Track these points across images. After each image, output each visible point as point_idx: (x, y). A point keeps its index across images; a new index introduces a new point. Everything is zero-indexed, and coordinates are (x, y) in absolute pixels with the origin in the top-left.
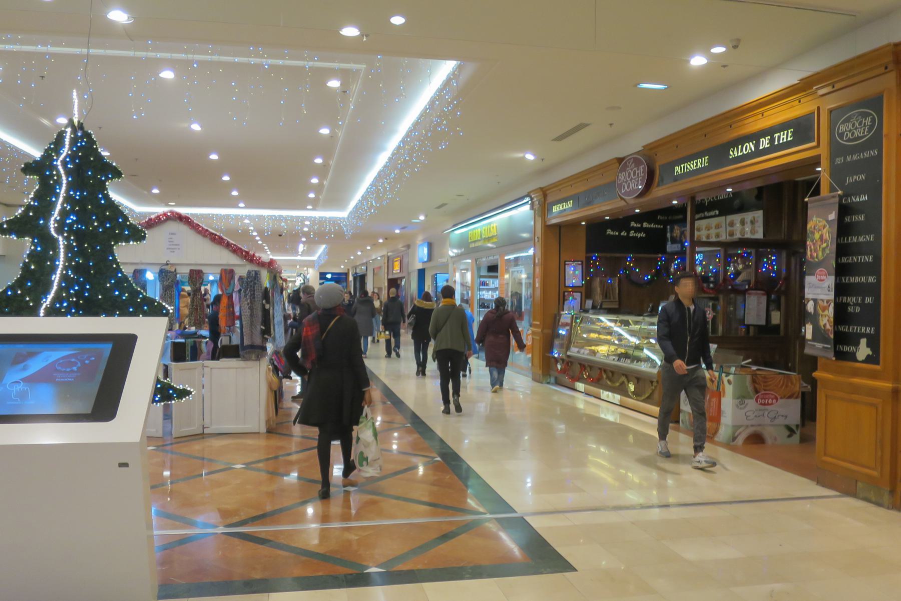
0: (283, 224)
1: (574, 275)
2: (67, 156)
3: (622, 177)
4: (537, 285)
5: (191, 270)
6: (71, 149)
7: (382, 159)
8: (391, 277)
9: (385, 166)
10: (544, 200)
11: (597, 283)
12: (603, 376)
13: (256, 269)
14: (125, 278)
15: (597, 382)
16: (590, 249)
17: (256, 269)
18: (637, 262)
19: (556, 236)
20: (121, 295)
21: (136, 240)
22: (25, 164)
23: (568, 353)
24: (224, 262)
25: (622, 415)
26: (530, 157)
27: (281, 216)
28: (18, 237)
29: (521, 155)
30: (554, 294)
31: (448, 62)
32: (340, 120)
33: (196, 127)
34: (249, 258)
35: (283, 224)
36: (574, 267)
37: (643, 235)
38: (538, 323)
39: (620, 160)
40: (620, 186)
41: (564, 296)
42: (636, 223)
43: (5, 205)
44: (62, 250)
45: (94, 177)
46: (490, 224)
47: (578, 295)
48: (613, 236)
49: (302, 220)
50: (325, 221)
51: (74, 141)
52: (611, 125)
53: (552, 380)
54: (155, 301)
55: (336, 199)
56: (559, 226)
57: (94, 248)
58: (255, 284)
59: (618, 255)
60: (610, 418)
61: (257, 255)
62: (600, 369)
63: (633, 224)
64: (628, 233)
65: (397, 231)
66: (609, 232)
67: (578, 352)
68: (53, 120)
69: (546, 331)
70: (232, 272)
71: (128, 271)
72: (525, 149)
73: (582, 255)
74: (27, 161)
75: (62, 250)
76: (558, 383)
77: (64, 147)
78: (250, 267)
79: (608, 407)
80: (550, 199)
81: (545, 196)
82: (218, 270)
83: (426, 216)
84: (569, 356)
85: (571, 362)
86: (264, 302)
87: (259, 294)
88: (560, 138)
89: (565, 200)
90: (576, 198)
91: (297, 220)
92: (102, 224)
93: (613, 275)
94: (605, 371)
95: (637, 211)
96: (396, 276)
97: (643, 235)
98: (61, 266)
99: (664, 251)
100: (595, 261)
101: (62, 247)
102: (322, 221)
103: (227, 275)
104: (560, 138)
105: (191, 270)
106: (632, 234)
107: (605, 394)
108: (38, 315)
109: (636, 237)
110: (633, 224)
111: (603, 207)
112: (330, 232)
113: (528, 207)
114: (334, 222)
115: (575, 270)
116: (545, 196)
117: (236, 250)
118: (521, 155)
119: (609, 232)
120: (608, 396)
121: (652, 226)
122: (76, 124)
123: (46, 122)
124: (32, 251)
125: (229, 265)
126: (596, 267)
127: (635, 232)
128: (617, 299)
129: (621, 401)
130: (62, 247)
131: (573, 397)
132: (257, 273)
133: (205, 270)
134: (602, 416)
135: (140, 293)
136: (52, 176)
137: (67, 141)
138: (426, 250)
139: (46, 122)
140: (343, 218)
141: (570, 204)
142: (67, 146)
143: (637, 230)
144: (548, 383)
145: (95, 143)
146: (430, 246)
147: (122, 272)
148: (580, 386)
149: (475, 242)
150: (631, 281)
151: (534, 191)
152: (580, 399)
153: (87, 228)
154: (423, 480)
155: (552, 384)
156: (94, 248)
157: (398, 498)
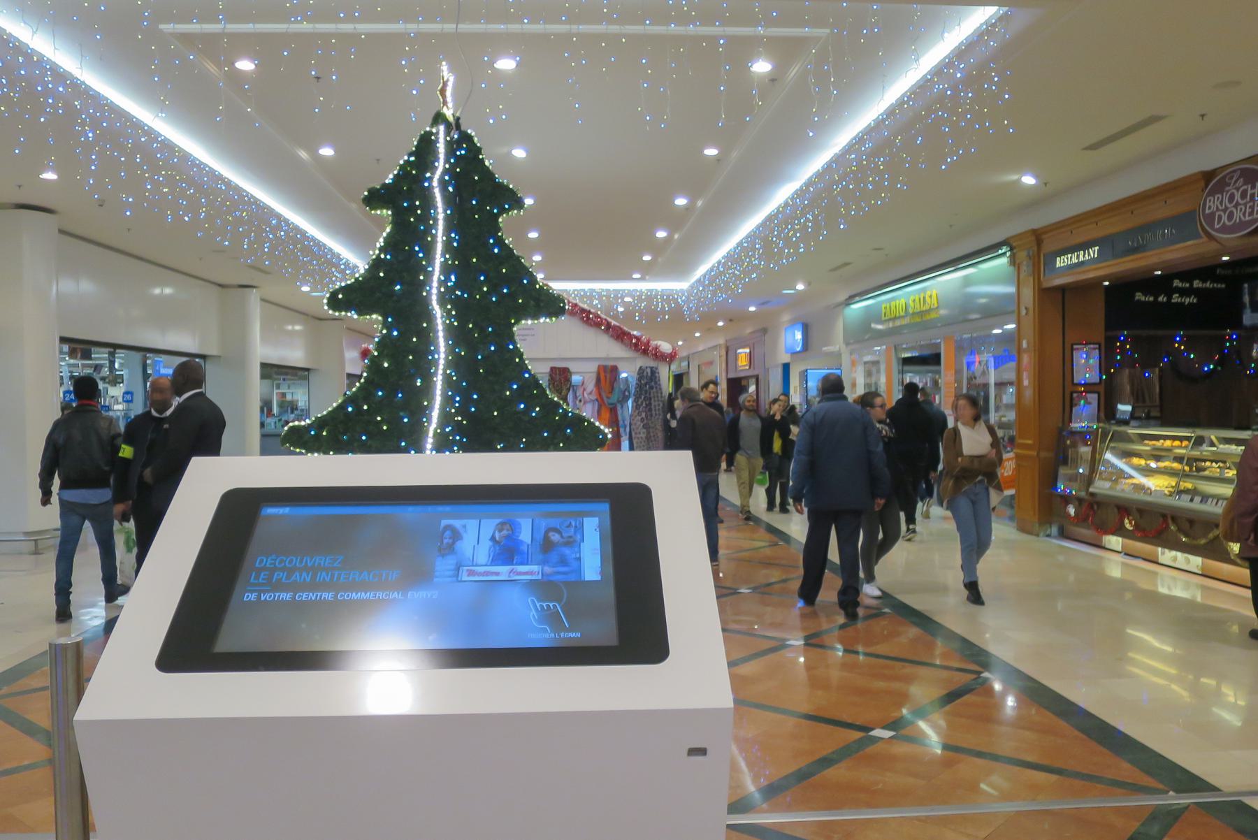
0: (596, 302)
1: (1086, 365)
2: (445, 172)
3: (1212, 204)
4: (1026, 383)
5: (552, 369)
6: (447, 161)
7: (782, 194)
8: (732, 375)
9: (786, 204)
10: (1033, 248)
11: (1124, 378)
12: (1157, 525)
13: (652, 364)
14: (534, 381)
15: (1142, 533)
16: (1109, 326)
17: (652, 364)
18: (1191, 343)
19: (1059, 304)
20: (529, 409)
21: (550, 315)
22: (369, 191)
23: (1091, 490)
24: (603, 355)
25: (1204, 588)
26: (1028, 180)
27: (593, 290)
28: (360, 314)
29: (1015, 177)
30: (1058, 392)
31: (987, 8)
32: (815, 114)
33: (519, 153)
34: (642, 348)
35: (596, 302)
36: (1087, 353)
37: (1193, 300)
38: (1030, 442)
39: (1208, 176)
40: (1210, 218)
41: (1072, 399)
42: (1182, 281)
43: (220, 285)
44: (441, 334)
45: (480, 208)
46: (924, 290)
47: (1093, 398)
48: (1145, 302)
49: (619, 295)
50: (656, 296)
51: (451, 150)
52: (1203, 116)
53: (1054, 530)
54: (582, 419)
55: (679, 267)
56: (1063, 290)
57: (482, 331)
58: (651, 388)
59: (1152, 332)
60: (1179, 592)
61: (653, 343)
62: (1164, 516)
63: (1177, 283)
64: (1170, 298)
65: (752, 309)
66: (1139, 296)
67: (1111, 488)
68: (313, 152)
69: (1044, 454)
70: (614, 371)
71: (539, 370)
72: (1022, 168)
73: (1100, 334)
74: (371, 186)
75: (441, 334)
76: (1064, 534)
77: (437, 160)
78: (647, 362)
79: (1178, 574)
80: (1048, 247)
81: (1039, 242)
82: (593, 367)
83: (809, 284)
84: (1092, 495)
85: (1098, 504)
86: (669, 416)
87: (657, 405)
88: (1093, 147)
89: (1085, 246)
90: (1109, 245)
91: (616, 297)
92: (495, 289)
93: (1147, 364)
94: (1174, 519)
95: (1225, 258)
96: (742, 375)
97: (1193, 300)
98: (442, 362)
99: (1237, 323)
100: (1123, 344)
101: (440, 327)
102: (650, 297)
103: (608, 375)
104: (1093, 147)
105: (552, 369)
106: (1176, 298)
107: (1167, 556)
108: (420, 450)
109: (1182, 304)
110: (1177, 283)
111: (1159, 257)
112: (663, 312)
113: (1004, 261)
114: (668, 297)
115: (1087, 359)
116: (1039, 242)
117: (620, 335)
118: (1015, 177)
119: (1139, 296)
120: (1175, 559)
121: (1208, 285)
122: (451, 119)
123: (303, 154)
124: (384, 337)
125: (608, 359)
126: (1123, 351)
127: (1181, 296)
128: (1158, 403)
129: (1203, 567)
130: (440, 327)
131: (1101, 558)
132: (654, 372)
133: (572, 367)
134: (1163, 590)
135: (558, 405)
136: (412, 209)
137: (441, 147)
138: (799, 336)
139: (303, 154)
140: (682, 291)
141: (1094, 252)
142: (442, 156)
143: (1183, 292)
144: (1048, 536)
145: (479, 150)
146: (806, 330)
147: (528, 371)
148: (1114, 541)
149: (895, 318)
150: (1180, 374)
151: (1020, 236)
152: (1115, 558)
153: (471, 296)
154: (1021, 722)
155: (1055, 537)
156: (482, 331)
157: (980, 754)
